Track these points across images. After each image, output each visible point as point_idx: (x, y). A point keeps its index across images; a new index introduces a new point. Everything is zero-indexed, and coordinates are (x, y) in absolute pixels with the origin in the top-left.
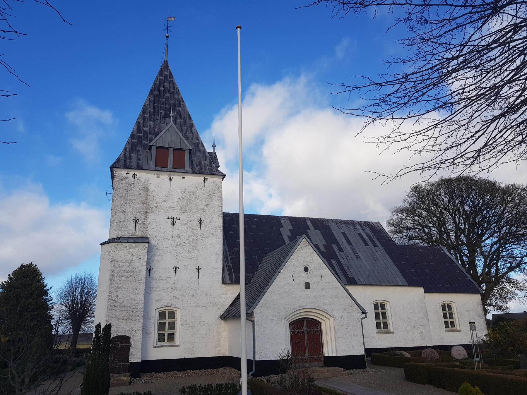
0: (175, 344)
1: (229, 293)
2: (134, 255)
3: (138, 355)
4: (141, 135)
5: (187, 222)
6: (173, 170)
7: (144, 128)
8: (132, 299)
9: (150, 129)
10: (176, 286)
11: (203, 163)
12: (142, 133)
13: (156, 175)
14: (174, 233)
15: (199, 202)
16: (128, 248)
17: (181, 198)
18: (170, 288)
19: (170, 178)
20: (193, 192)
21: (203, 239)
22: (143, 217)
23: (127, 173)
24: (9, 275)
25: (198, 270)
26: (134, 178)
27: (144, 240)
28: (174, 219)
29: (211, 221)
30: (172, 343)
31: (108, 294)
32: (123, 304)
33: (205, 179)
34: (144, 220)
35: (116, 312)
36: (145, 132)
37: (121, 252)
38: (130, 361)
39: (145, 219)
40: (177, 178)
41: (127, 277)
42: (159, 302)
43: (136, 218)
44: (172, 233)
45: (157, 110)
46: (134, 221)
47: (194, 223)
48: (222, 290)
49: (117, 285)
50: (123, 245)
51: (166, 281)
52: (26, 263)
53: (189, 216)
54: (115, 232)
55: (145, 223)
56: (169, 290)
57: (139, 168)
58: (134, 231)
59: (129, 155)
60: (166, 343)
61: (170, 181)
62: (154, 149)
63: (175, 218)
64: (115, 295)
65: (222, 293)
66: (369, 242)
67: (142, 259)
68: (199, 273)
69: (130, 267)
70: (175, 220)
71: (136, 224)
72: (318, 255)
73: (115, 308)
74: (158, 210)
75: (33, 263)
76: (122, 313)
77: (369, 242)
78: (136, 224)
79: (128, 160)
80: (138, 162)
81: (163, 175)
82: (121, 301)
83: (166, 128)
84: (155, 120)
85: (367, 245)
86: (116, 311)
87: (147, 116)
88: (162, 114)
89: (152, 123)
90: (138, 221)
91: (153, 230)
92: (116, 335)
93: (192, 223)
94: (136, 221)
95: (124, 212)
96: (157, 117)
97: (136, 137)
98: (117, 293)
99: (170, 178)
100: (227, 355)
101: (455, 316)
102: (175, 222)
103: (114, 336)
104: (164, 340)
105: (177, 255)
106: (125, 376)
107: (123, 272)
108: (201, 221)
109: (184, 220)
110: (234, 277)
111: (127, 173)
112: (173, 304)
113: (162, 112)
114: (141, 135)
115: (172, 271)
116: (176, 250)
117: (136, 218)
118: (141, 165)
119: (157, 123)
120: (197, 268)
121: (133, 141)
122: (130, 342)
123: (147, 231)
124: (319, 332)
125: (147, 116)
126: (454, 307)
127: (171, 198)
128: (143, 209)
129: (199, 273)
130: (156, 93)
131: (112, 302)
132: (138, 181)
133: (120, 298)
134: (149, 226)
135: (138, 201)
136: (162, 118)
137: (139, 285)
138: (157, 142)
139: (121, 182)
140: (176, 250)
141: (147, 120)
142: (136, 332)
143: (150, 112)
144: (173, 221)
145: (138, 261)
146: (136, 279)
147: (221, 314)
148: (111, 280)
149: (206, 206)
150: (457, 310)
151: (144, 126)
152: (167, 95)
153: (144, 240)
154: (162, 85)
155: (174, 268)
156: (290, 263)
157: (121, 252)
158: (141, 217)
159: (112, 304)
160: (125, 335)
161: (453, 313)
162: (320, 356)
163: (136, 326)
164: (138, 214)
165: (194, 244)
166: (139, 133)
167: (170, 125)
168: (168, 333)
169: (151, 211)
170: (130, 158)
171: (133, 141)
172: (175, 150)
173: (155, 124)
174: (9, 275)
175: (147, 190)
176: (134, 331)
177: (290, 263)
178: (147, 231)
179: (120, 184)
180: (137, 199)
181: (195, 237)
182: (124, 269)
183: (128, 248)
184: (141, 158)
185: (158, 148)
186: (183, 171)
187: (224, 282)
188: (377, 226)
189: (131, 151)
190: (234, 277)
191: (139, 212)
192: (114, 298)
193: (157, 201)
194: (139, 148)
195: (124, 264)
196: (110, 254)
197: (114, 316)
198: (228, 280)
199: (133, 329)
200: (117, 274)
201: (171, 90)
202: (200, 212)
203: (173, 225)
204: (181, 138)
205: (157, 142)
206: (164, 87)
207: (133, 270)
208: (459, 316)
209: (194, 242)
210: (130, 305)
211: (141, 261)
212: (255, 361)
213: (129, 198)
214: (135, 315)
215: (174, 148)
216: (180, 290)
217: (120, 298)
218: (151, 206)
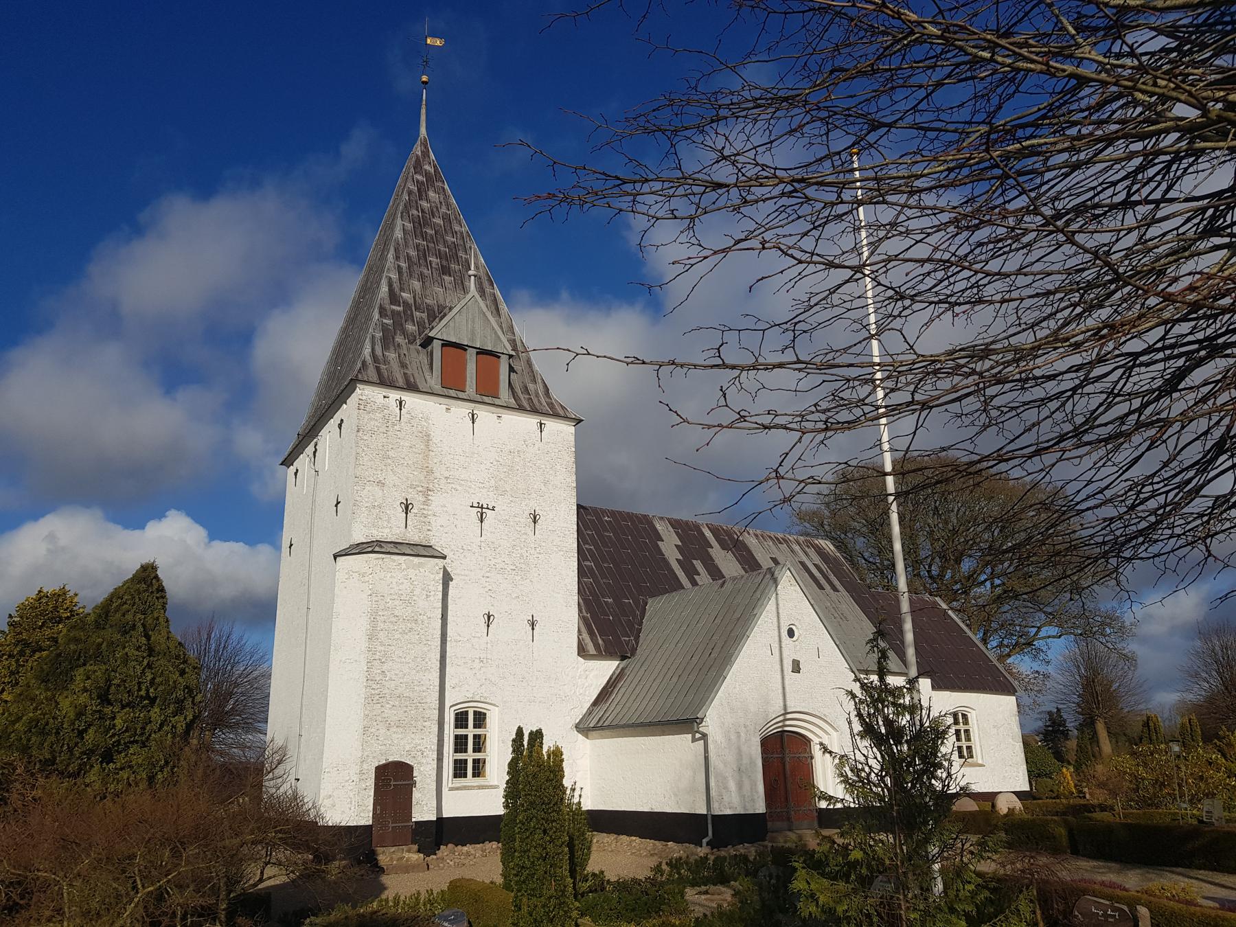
0: (486, 784)
1: (591, 676)
2: (416, 583)
3: (429, 805)
4: (398, 308)
5: (507, 517)
6: (478, 398)
7: (402, 294)
8: (416, 683)
9: (414, 297)
10: (489, 657)
11: (531, 386)
12: (399, 306)
13: (445, 407)
14: (483, 539)
15: (532, 474)
16: (404, 566)
17: (495, 463)
18: (478, 661)
19: (473, 415)
20: (519, 451)
21: (539, 556)
22: (422, 499)
23: (385, 397)
24: (10, 616)
25: (533, 625)
26: (401, 409)
27: (423, 550)
28: (482, 508)
29: (555, 519)
30: (478, 781)
31: (365, 669)
32: (397, 692)
33: (541, 424)
34: (422, 507)
35: (383, 709)
36: (406, 304)
37: (390, 575)
38: (414, 820)
39: (425, 503)
40: (485, 415)
41: (404, 633)
42: (457, 689)
43: (407, 500)
44: (479, 539)
45: (423, 254)
46: (403, 506)
47: (522, 520)
48: (578, 669)
49: (383, 648)
50: (394, 561)
51: (470, 645)
52: (49, 588)
53: (513, 504)
54: (364, 529)
55: (425, 512)
56: (477, 664)
57: (411, 387)
58: (403, 529)
59: (381, 354)
60: (470, 780)
61: (473, 423)
62: (436, 345)
63: (485, 506)
64: (379, 671)
65: (578, 675)
66: (823, 581)
67: (433, 593)
68: (533, 629)
69: (410, 609)
70: (484, 510)
71: (407, 513)
72: (812, 605)
73: (381, 700)
74: (451, 486)
75: (67, 588)
76: (395, 712)
77: (823, 581)
78: (407, 513)
79: (382, 366)
80: (405, 374)
81: (459, 407)
82: (393, 684)
83: (463, 302)
84: (422, 277)
85: (821, 587)
86: (382, 706)
87: (404, 265)
88: (433, 265)
89: (416, 285)
90: (410, 507)
91: (442, 529)
92: (384, 762)
93: (517, 519)
94: (407, 508)
95: (381, 484)
96: (425, 271)
97: (389, 313)
98: (385, 667)
99: (473, 415)
100: (590, 809)
101: (974, 735)
102: (484, 515)
103: (381, 763)
104: (465, 776)
105: (491, 588)
106: (409, 851)
107: (394, 619)
108: (535, 518)
109: (502, 512)
110: (600, 642)
111: (385, 397)
112: (485, 695)
113: (434, 260)
114: (398, 308)
115: (482, 621)
116: (488, 577)
117: (407, 500)
118: (412, 380)
119: (427, 284)
120: (531, 619)
121: (385, 321)
122: (413, 777)
123: (429, 530)
124: (809, 760)
125: (404, 265)
126: (972, 717)
127: (475, 460)
128: (421, 481)
129: (533, 629)
130: (415, 212)
131: (374, 686)
132: (409, 416)
133: (391, 679)
134: (432, 519)
135: (410, 462)
136: (434, 274)
137: (429, 651)
138: (441, 331)
139: (373, 417)
140: (488, 577)
141: (405, 275)
142: (425, 754)
143: (409, 257)
144: (482, 511)
145: (425, 596)
146: (423, 637)
147: (577, 721)
148: (371, 637)
149: (545, 484)
150: (978, 724)
151: (402, 289)
152: (439, 221)
153: (423, 550)
154: (424, 195)
155: (486, 616)
156: (766, 619)
157: (390, 575)
158: (417, 499)
159: (373, 692)
160: (403, 760)
161: (971, 730)
162: (811, 808)
163: (425, 740)
164: (410, 490)
165: (523, 566)
166: (394, 305)
167: (469, 296)
168: (474, 760)
169: (437, 486)
170: (386, 362)
171: (385, 321)
172: (481, 352)
173: (424, 287)
174: (10, 616)
175: (427, 438)
176: (419, 753)
177: (766, 619)
178: (429, 530)
179: (371, 419)
180: (407, 458)
181: (523, 551)
182: (396, 613)
183: (404, 566)
184: (408, 363)
185: (447, 344)
186: (461, 395)
187: (582, 651)
188: (828, 549)
189: (385, 347)
190: (600, 642)
191: (412, 486)
192: (378, 679)
193: (448, 465)
194: (399, 339)
195: (397, 602)
196: (366, 579)
197: (379, 718)
198: (591, 649)
199: (419, 747)
200: (382, 625)
201: (444, 209)
202: (534, 495)
203: (482, 522)
204: (493, 329)
205: (441, 331)
206: (428, 200)
207: (415, 618)
208: (981, 736)
209: (522, 561)
210: (411, 695)
211: (432, 598)
212: (713, 816)
213: (391, 453)
214: (423, 717)
215: (479, 348)
216: (498, 666)
217: (391, 679)
218: (437, 475)
